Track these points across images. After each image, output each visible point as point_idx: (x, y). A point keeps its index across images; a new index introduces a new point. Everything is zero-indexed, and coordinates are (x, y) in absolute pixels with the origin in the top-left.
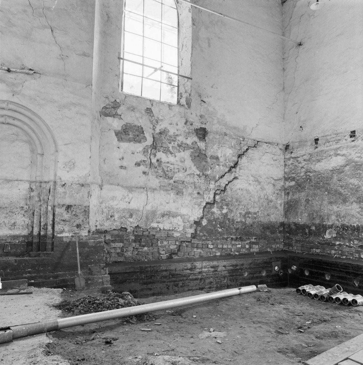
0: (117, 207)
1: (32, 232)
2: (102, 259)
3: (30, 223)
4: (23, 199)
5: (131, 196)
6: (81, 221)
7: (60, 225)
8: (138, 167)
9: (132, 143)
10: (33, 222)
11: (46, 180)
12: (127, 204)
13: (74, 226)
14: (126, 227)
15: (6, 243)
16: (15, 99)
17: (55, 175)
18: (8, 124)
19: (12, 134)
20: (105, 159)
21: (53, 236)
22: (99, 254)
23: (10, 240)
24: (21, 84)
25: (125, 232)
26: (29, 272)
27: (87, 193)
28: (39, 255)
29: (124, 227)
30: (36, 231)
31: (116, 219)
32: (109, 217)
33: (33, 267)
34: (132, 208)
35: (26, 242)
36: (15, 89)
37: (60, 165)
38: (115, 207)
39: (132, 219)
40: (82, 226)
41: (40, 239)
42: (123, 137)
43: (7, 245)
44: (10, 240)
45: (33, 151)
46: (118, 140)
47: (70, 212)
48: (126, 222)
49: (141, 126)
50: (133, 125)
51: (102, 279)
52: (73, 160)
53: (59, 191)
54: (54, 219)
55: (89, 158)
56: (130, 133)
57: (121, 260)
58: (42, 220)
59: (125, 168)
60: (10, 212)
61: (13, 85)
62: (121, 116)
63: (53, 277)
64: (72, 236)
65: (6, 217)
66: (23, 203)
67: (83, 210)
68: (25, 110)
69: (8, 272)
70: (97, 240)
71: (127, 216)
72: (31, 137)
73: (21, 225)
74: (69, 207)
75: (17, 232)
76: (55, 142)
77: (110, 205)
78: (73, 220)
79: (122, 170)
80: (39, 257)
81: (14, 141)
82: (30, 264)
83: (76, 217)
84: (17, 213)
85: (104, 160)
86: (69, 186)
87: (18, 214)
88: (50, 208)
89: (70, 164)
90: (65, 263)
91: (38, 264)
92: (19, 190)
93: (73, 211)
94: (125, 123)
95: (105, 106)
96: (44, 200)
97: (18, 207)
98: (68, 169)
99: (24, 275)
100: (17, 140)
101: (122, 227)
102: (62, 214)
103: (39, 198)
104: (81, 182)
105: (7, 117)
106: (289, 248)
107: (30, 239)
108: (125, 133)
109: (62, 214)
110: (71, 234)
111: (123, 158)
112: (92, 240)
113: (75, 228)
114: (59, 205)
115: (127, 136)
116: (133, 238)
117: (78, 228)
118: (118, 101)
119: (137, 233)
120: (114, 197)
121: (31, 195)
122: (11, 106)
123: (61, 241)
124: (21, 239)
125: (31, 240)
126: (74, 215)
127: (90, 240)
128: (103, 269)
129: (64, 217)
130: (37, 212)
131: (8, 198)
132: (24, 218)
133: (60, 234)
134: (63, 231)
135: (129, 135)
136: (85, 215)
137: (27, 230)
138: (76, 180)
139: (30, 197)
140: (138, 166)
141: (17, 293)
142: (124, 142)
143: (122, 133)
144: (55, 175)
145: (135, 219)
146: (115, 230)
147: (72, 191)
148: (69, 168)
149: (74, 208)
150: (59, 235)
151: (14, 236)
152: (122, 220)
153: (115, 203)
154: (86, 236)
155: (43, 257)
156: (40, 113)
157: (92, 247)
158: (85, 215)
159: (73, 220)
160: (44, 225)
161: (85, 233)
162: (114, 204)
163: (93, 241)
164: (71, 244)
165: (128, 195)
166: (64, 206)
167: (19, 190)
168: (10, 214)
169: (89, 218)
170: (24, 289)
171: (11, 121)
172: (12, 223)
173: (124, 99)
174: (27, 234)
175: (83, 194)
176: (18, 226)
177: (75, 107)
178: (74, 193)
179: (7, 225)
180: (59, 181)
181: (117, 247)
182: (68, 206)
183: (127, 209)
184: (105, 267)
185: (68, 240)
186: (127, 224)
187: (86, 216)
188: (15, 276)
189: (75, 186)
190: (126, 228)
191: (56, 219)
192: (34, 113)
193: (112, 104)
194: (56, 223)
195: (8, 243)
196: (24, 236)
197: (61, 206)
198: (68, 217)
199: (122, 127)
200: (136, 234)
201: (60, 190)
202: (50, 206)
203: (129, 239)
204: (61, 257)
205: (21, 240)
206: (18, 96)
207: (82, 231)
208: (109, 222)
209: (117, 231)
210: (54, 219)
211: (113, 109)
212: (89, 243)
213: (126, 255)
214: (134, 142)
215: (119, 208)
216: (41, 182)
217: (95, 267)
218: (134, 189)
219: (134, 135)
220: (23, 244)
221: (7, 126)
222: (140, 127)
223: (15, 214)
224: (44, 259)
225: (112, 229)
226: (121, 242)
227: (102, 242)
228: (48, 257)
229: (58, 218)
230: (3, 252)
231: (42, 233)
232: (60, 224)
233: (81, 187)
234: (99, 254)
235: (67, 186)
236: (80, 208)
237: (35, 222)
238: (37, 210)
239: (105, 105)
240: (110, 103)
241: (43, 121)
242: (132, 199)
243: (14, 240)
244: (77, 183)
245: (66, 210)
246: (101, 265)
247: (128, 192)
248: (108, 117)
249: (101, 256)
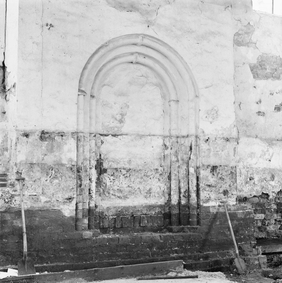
0: (256, 166)
1: (169, 200)
2: (253, 235)
3: (166, 190)
4: (157, 158)
5: (271, 151)
6: (228, 186)
7: (205, 192)
8: (278, 113)
9: (270, 80)
10: (170, 188)
11: (185, 134)
12: (268, 162)
13: (221, 193)
14: (267, 193)
15: (141, 215)
16: (150, 32)
17: (197, 127)
18: (137, 63)
19: (140, 76)
20: (241, 103)
21: (199, 206)
22: (249, 228)
23: (146, 212)
24: (155, 11)
25: (266, 200)
26: (176, 252)
27: (233, 150)
28: (182, 230)
29: (265, 193)
30: (174, 200)
31: (256, 183)
32: (248, 180)
33: (180, 245)
34: (273, 168)
35: (163, 214)
36: (149, 19)
37: (202, 114)
38: (254, 166)
39: (274, 182)
40: (229, 192)
41: (179, 210)
42: (259, 72)
43: (143, 218)
44: (146, 212)
45: (164, 97)
46: (254, 77)
47: (215, 174)
48: (268, 186)
49: (279, 56)
50: (270, 55)
51: (259, 261)
52: (215, 106)
53: (203, 148)
54: (198, 185)
55: (233, 103)
56: (268, 67)
57: (262, 236)
58: (182, 185)
59: (264, 114)
60: (144, 175)
61: (148, 13)
62: (256, 44)
63: (203, 257)
64: (219, 206)
65: (141, 183)
66: (157, 164)
67: (229, 172)
68: (161, 45)
69: (155, 251)
70: (246, 211)
71: (269, 178)
72: (162, 79)
73: (157, 191)
74: (214, 168)
75: (152, 201)
76: (194, 84)
77: (248, 164)
78: (219, 185)
79: (260, 117)
80: (184, 232)
81: (143, 85)
82: (177, 241)
83: (222, 181)
84: (152, 177)
85: (240, 105)
86: (213, 141)
87: (153, 178)
88: (192, 170)
89: (212, 113)
90: (213, 240)
91: (184, 241)
92: (153, 147)
93: (219, 173)
94: (261, 54)
95: (237, 32)
96: (183, 160)
97: (152, 169)
98: (211, 120)
99: (172, 255)
100: (146, 83)
101: (263, 193)
102: (207, 177)
103: (177, 157)
104: (226, 135)
105: (137, 54)
106: (273, 238)
107: (167, 210)
108: (261, 66)
109: (207, 177)
110: (218, 203)
111: (260, 102)
112: (241, 210)
113: (222, 195)
114: (203, 165)
115: (264, 71)
116: (275, 207)
117: (225, 195)
118: (251, 23)
119: (279, 200)
120: (252, 153)
121: (166, 154)
122: (146, 41)
123: (208, 213)
124: (157, 210)
125: (168, 211)
126: (220, 178)
127: (238, 210)
128: (254, 247)
129: (209, 182)
130: (176, 175)
131: (141, 158)
132: (159, 184)
133: (207, 203)
134: (209, 199)
135: (266, 69)
136: (232, 178)
137: (163, 198)
138: (220, 132)
139: (164, 156)
140: (278, 110)
141: (176, 278)
142: (261, 79)
143: (257, 67)
144: (197, 127)
145: (277, 182)
146: (255, 196)
147: (216, 148)
148: (212, 117)
149: (219, 170)
150: (205, 205)
151: (150, 206)
152: (263, 183)
153: (254, 161)
154: (233, 205)
155: (189, 233)
156: (178, 48)
157: (242, 219)
158: (232, 178)
159: (219, 185)
160: (185, 192)
161: (233, 201)
162: (252, 162)
163: (242, 211)
164: (218, 216)
165: (268, 151)
166: (209, 167)
167: (153, 147)
168: (145, 179)
169: (236, 182)
170: (181, 272)
171: (141, 59)
172: (148, 189)
173: (258, 21)
174: (163, 204)
175: (228, 151)
176: (153, 194)
177: (215, 37)
178: (218, 150)
179: (142, 193)
180: (201, 135)
181: (258, 219)
182: (213, 167)
183: (267, 169)
184: (256, 245)
185: (215, 211)
186: (269, 189)
187: (233, 180)
188: (162, 256)
189: (219, 142)
190: (267, 194)
191: (201, 185)
192: (170, 48)
193: (245, 29)
194: (201, 189)
195: (144, 214)
196: (161, 206)
197: (206, 167)
198: (214, 181)
199: (258, 59)
200: (279, 201)
201: (204, 146)
202: (193, 167)
203: (271, 208)
204: (207, 233)
205: (157, 212)
206: (153, 27)
207: (230, 199)
208: (248, 186)
209: (257, 198)
210: (198, 185)
211: (246, 35)
212: (238, 215)
213: (269, 230)
214: (272, 78)
215: (259, 168)
216: (178, 137)
217: (246, 246)
218: (274, 142)
219: (272, 69)
220: (160, 217)
221: (135, 66)
222: (278, 58)
223: (150, 179)
224: (190, 235)
225: (253, 195)
226: (262, 213)
227: (252, 213)
228: (194, 232)
229: (203, 183)
230: (140, 226)
231: (183, 202)
232: (205, 190)
233: (226, 142)
234: (249, 228)
235: (211, 142)
236: (226, 170)
237: (174, 188)
238: (176, 173)
239: (237, 31)
240: (243, 28)
241: (181, 58)
242: (272, 155)
243: (150, 211)
244: (222, 136)
245: (211, 172)
246: (252, 242)
247: (267, 146)
248: (241, 47)
249: (252, 231)
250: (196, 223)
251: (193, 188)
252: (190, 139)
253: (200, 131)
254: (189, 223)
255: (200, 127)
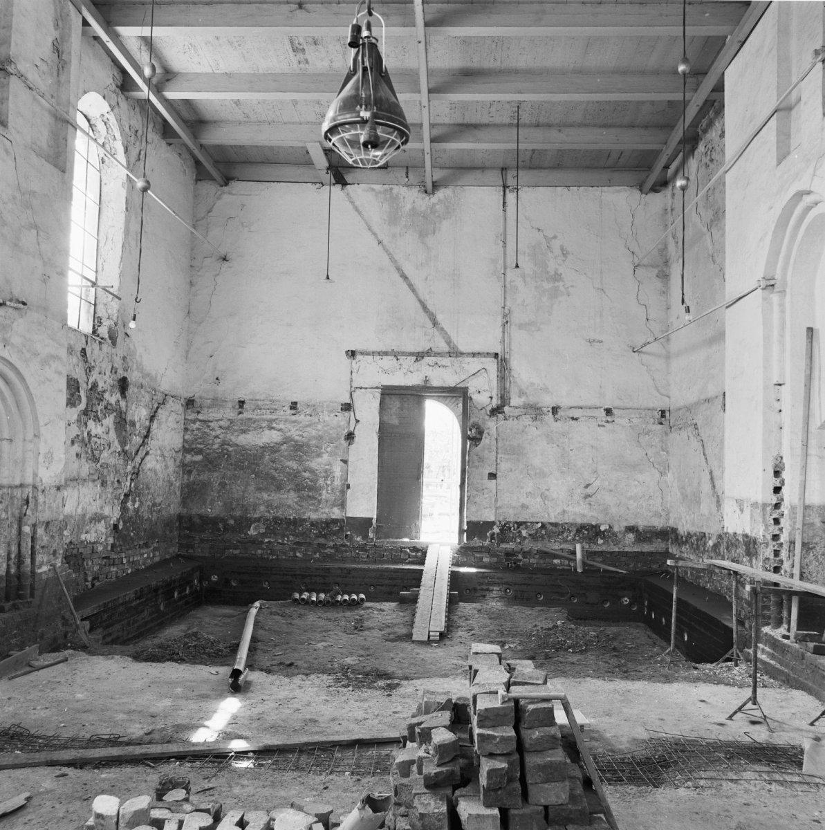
17: (35, 475)
21: (33, 573)
54: (33, 548)
67: (58, 528)
98: (47, 465)
144: (35, 475)
241: (27, 388)
250: (28, 596)
251: (26, 551)
252: (27, 489)
253: (38, 479)
254: (19, 597)
255: (39, 475)
